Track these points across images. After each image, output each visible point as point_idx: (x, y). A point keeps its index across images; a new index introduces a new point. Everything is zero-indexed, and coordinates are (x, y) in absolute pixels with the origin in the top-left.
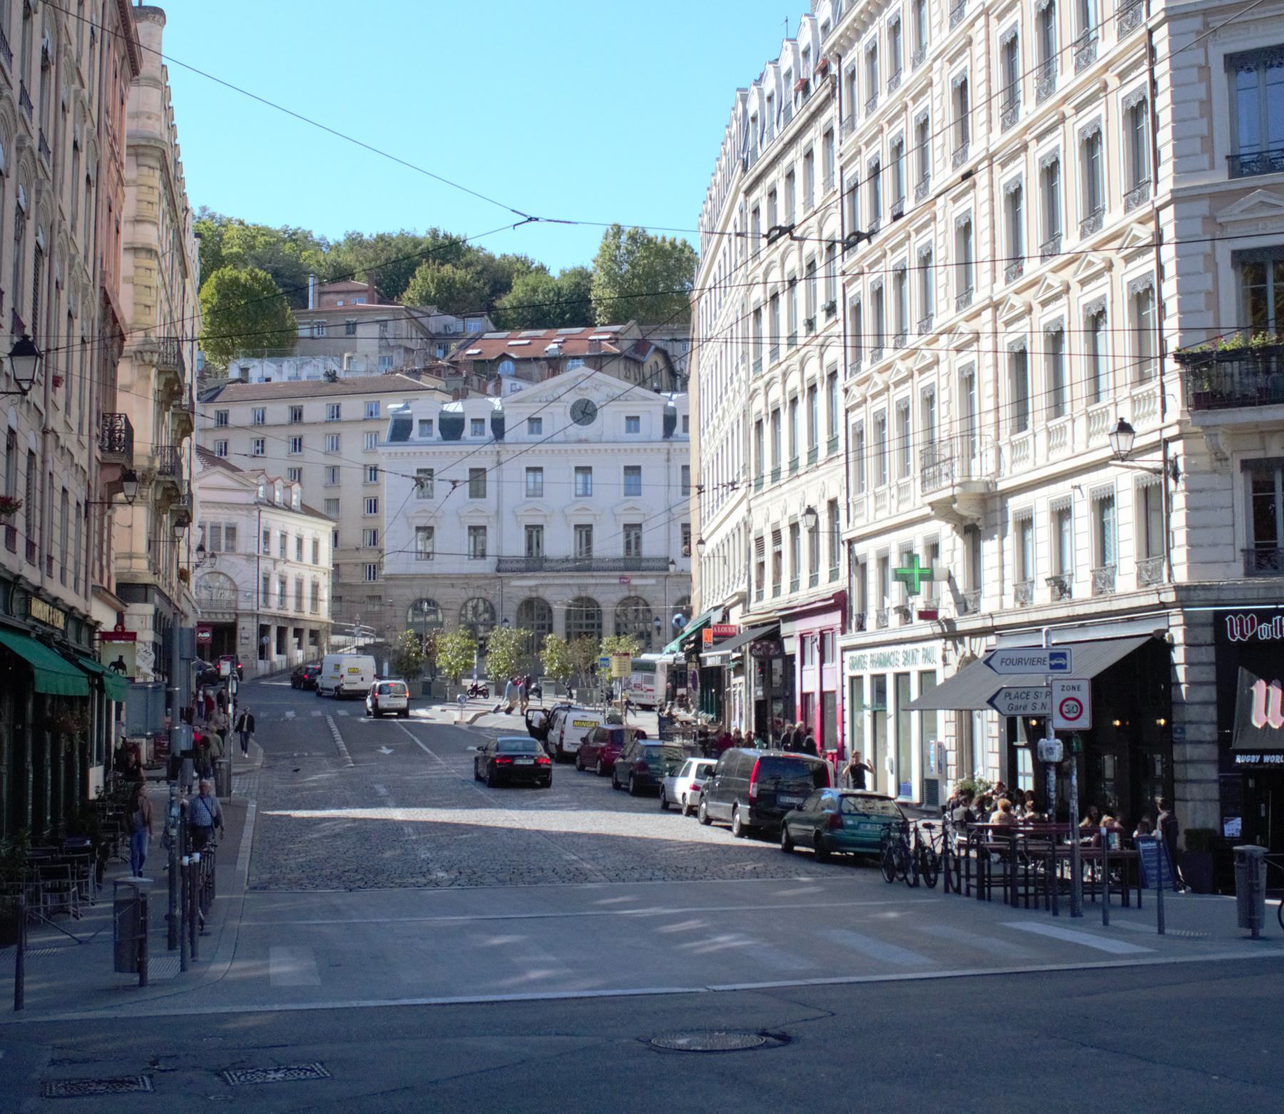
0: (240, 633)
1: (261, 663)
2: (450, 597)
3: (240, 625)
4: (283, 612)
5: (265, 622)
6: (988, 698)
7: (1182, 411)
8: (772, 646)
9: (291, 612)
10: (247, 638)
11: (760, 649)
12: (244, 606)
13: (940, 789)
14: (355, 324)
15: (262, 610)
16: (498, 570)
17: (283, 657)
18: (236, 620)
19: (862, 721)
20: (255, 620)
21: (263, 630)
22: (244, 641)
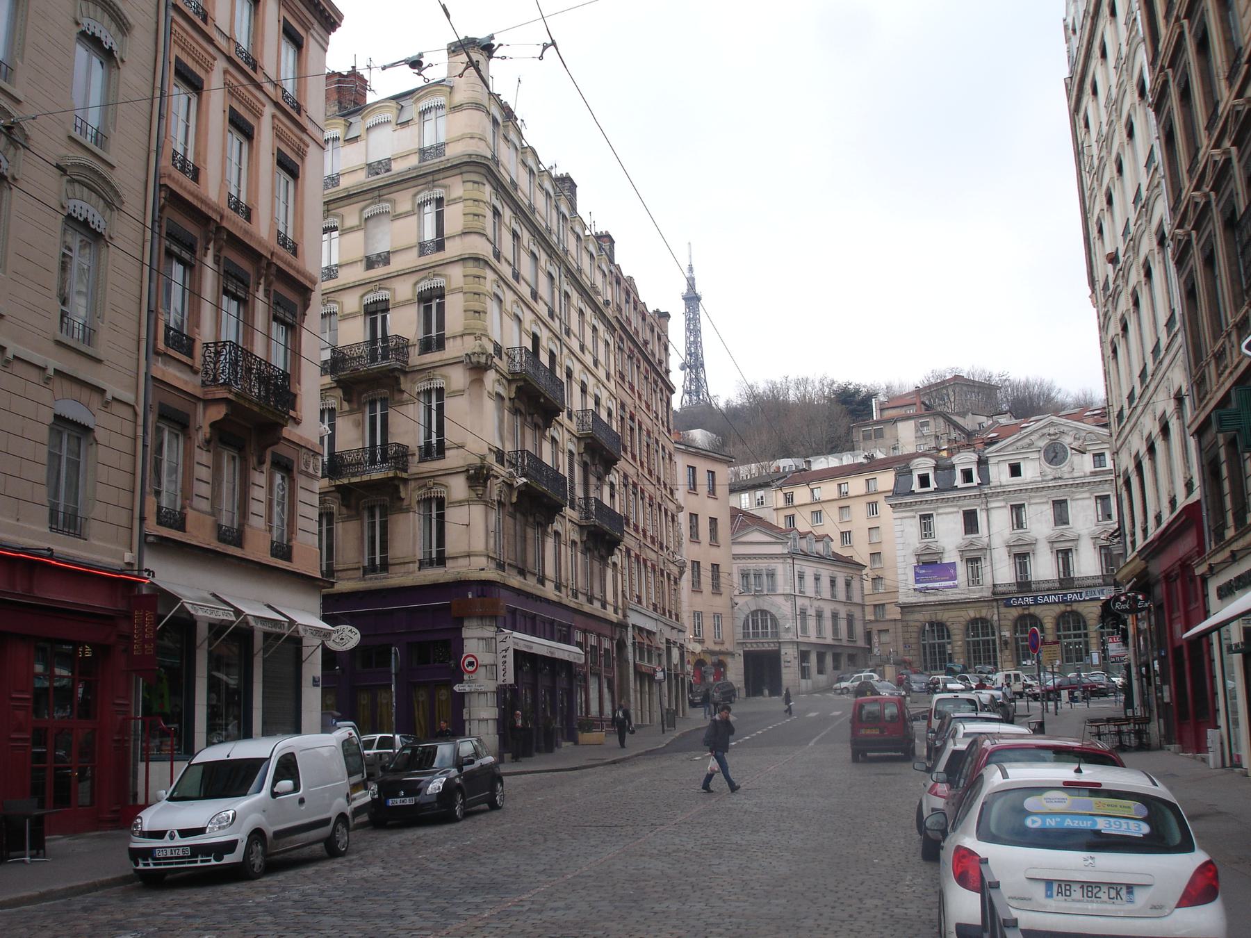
0: (783, 658)
1: (803, 682)
2: (956, 620)
3: (783, 652)
4: (806, 640)
5: (804, 648)
6: (699, 516)
7: (805, 381)
8: (1140, 597)
9: (813, 638)
10: (789, 662)
11: (1124, 602)
12: (785, 637)
13: (1068, 761)
14: (930, 516)
15: (800, 639)
16: (994, 593)
17: (809, 682)
18: (780, 647)
19: (1232, 665)
20: (795, 647)
21: (804, 656)
22: (787, 664)
